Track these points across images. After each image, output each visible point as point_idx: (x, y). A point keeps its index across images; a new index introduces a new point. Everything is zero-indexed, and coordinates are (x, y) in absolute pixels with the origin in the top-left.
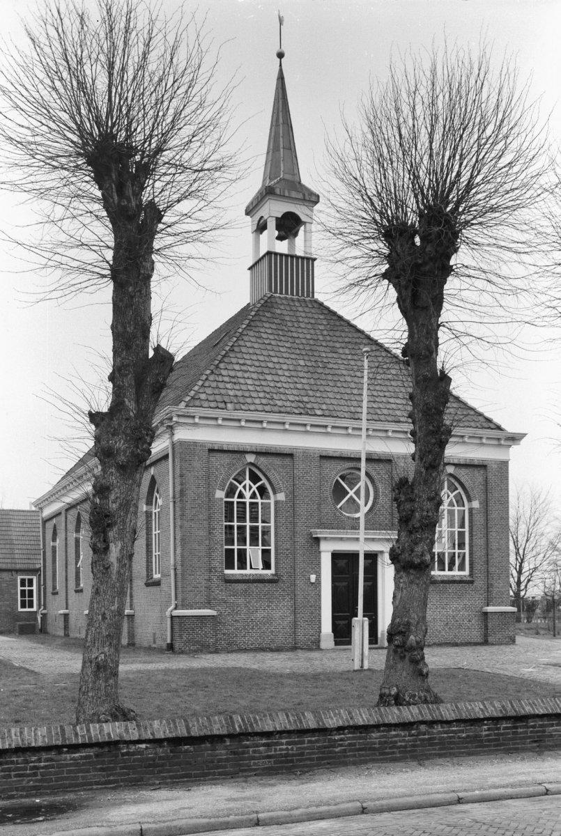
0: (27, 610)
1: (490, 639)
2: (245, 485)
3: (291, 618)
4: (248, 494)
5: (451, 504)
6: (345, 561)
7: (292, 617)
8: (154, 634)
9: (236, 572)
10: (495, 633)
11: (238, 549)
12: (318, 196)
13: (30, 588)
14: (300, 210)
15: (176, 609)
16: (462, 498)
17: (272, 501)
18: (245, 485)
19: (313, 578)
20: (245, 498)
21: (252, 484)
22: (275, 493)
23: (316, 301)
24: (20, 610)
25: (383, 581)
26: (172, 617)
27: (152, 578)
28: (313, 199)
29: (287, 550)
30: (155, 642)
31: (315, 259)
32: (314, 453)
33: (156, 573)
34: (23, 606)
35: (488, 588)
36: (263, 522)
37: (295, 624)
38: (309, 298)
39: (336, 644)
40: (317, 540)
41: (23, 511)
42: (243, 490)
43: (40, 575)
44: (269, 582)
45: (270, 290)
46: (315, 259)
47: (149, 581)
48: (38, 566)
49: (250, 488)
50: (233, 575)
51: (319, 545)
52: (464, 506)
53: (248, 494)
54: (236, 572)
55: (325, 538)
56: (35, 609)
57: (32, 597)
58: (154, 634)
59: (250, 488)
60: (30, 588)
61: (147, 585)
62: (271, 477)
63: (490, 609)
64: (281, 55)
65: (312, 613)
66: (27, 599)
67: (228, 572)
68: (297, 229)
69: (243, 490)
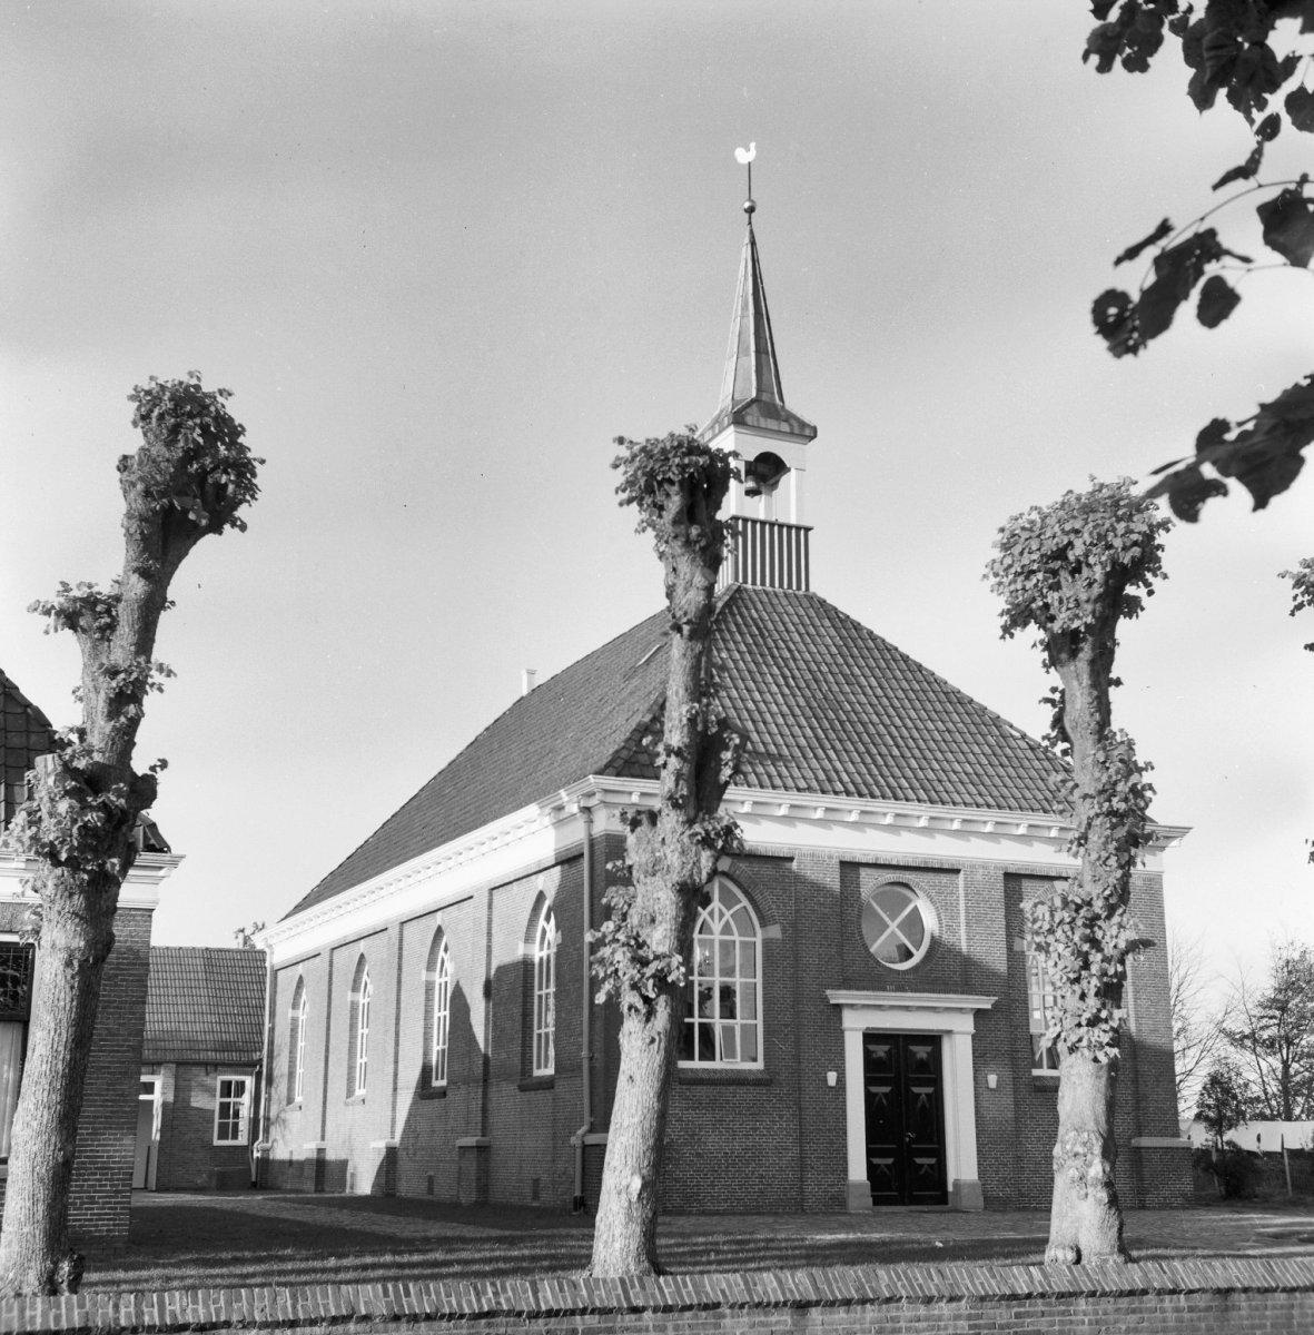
0: (229, 1142)
1: (1149, 1199)
2: (713, 910)
3: (794, 1152)
4: (717, 926)
5: (726, 930)
6: (886, 1048)
7: (796, 1150)
8: (536, 1182)
9: (697, 1064)
10: (1157, 1188)
11: (700, 1024)
12: (815, 429)
13: (226, 1100)
14: (784, 449)
15: (591, 1131)
16: (750, 919)
17: (758, 940)
18: (713, 910)
19: (832, 1078)
20: (711, 933)
21: (724, 909)
22: (763, 925)
23: (811, 598)
24: (217, 1142)
25: (954, 1081)
26: (585, 1147)
27: (531, 1076)
28: (807, 432)
29: (786, 1026)
30: (536, 1196)
31: (808, 530)
32: (830, 857)
33: (437, 1079)
34: (223, 1136)
35: (1138, 1102)
36: (701, 975)
37: (802, 1164)
38: (790, 591)
39: (877, 1201)
40: (838, 1008)
41: (229, 951)
42: (709, 919)
43: (259, 1075)
44: (755, 1085)
45: (737, 579)
46: (808, 530)
47: (524, 1082)
48: (256, 1056)
49: (722, 915)
50: (692, 1070)
51: (840, 1019)
52: (755, 935)
53: (717, 926)
54: (697, 1064)
55: (852, 1006)
56: (242, 1140)
57: (220, 1125)
58: (536, 1182)
59: (722, 915)
60: (226, 1100)
61: (523, 1089)
62: (758, 897)
63: (1146, 1142)
64: (751, 210)
65: (832, 1143)
66: (231, 1120)
67: (683, 1064)
68: (777, 478)
69: (709, 919)
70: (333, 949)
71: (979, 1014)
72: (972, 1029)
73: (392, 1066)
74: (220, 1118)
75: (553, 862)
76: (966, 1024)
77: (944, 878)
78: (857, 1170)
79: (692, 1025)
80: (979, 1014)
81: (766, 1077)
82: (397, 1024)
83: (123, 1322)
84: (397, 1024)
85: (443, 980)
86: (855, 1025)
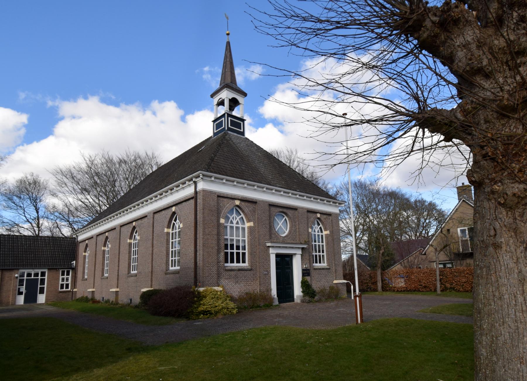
5: (237, 223)
9: (235, 264)
20: (233, 223)
49: (236, 219)
53: (235, 222)
59: (233, 218)
70: (97, 236)
71: (303, 249)
72: (301, 253)
73: (117, 268)
74: (44, 287)
75: (218, 86)
76: (299, 252)
77: (92, 285)
78: (274, 292)
79: (228, 252)
80: (303, 249)
81: (249, 268)
82: (119, 255)
83: (297, 170)
84: (119, 255)
85: (135, 242)
86: (273, 253)
